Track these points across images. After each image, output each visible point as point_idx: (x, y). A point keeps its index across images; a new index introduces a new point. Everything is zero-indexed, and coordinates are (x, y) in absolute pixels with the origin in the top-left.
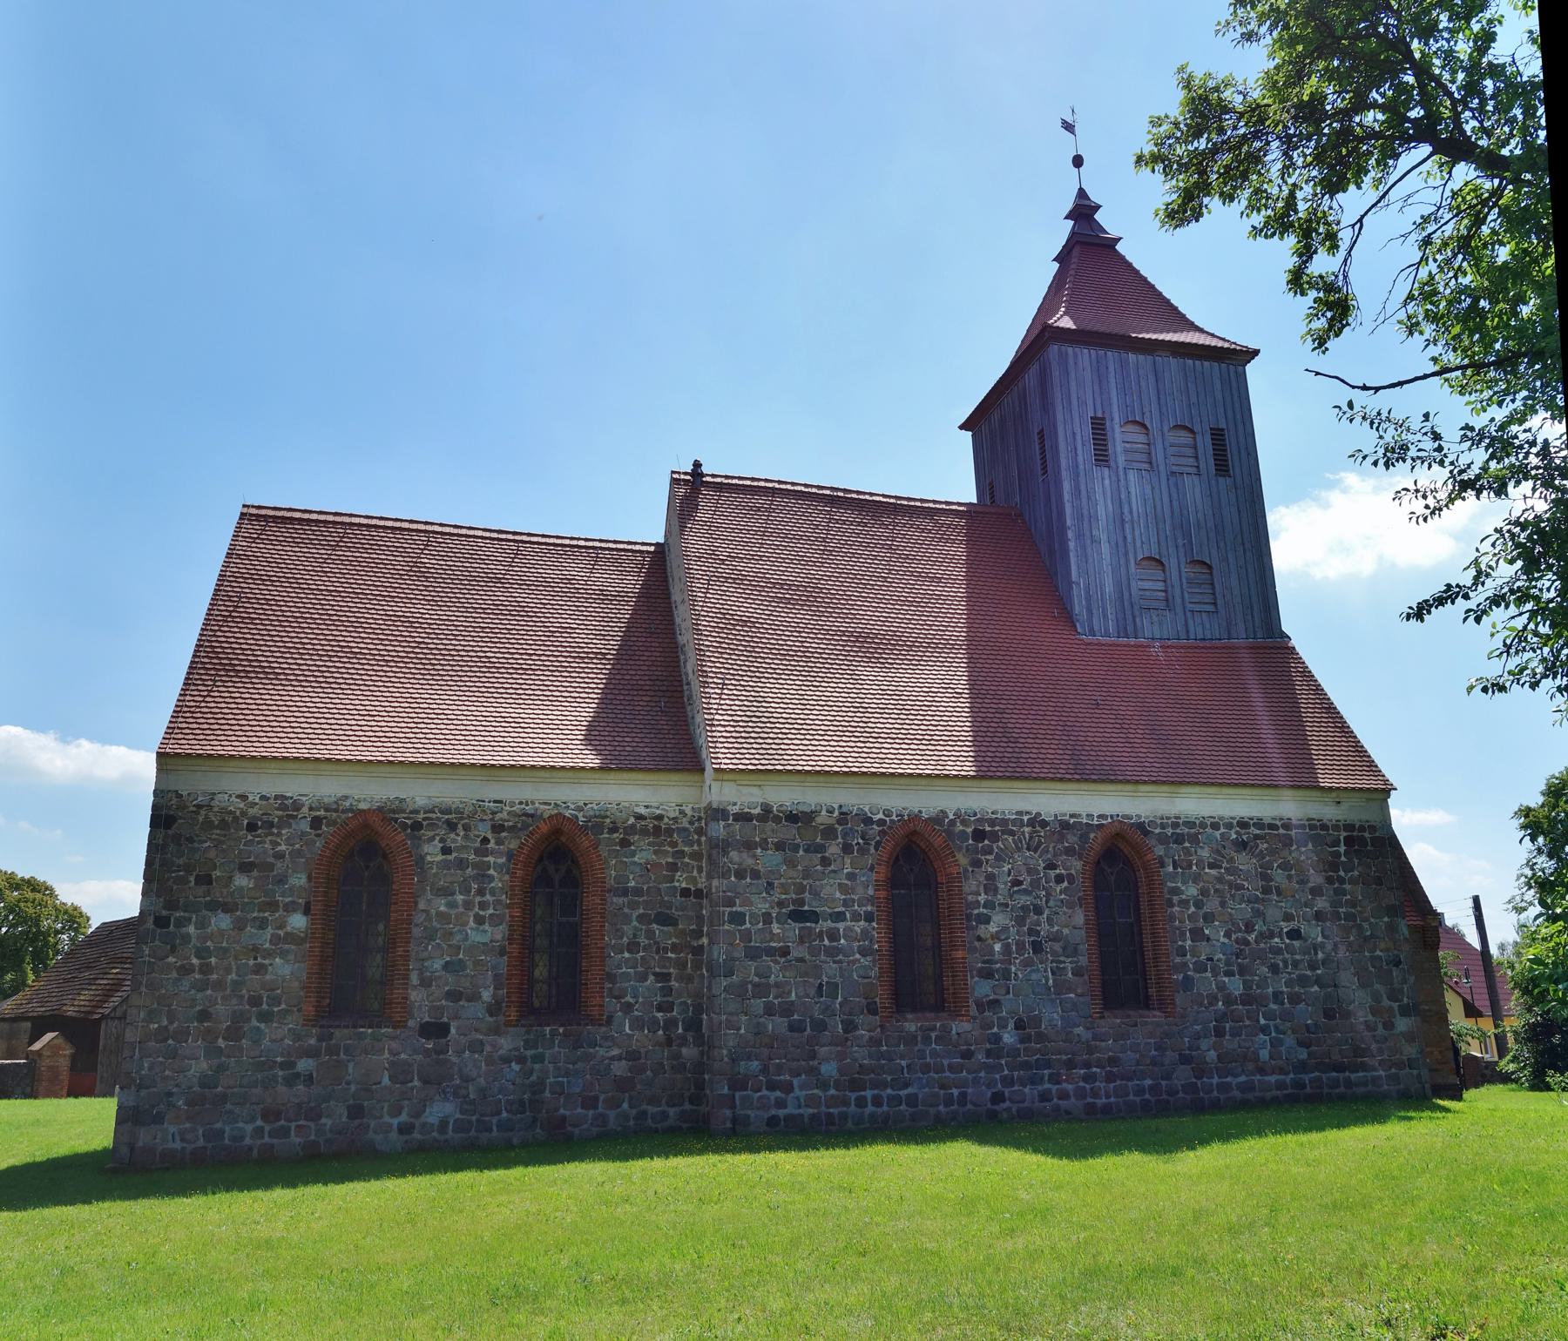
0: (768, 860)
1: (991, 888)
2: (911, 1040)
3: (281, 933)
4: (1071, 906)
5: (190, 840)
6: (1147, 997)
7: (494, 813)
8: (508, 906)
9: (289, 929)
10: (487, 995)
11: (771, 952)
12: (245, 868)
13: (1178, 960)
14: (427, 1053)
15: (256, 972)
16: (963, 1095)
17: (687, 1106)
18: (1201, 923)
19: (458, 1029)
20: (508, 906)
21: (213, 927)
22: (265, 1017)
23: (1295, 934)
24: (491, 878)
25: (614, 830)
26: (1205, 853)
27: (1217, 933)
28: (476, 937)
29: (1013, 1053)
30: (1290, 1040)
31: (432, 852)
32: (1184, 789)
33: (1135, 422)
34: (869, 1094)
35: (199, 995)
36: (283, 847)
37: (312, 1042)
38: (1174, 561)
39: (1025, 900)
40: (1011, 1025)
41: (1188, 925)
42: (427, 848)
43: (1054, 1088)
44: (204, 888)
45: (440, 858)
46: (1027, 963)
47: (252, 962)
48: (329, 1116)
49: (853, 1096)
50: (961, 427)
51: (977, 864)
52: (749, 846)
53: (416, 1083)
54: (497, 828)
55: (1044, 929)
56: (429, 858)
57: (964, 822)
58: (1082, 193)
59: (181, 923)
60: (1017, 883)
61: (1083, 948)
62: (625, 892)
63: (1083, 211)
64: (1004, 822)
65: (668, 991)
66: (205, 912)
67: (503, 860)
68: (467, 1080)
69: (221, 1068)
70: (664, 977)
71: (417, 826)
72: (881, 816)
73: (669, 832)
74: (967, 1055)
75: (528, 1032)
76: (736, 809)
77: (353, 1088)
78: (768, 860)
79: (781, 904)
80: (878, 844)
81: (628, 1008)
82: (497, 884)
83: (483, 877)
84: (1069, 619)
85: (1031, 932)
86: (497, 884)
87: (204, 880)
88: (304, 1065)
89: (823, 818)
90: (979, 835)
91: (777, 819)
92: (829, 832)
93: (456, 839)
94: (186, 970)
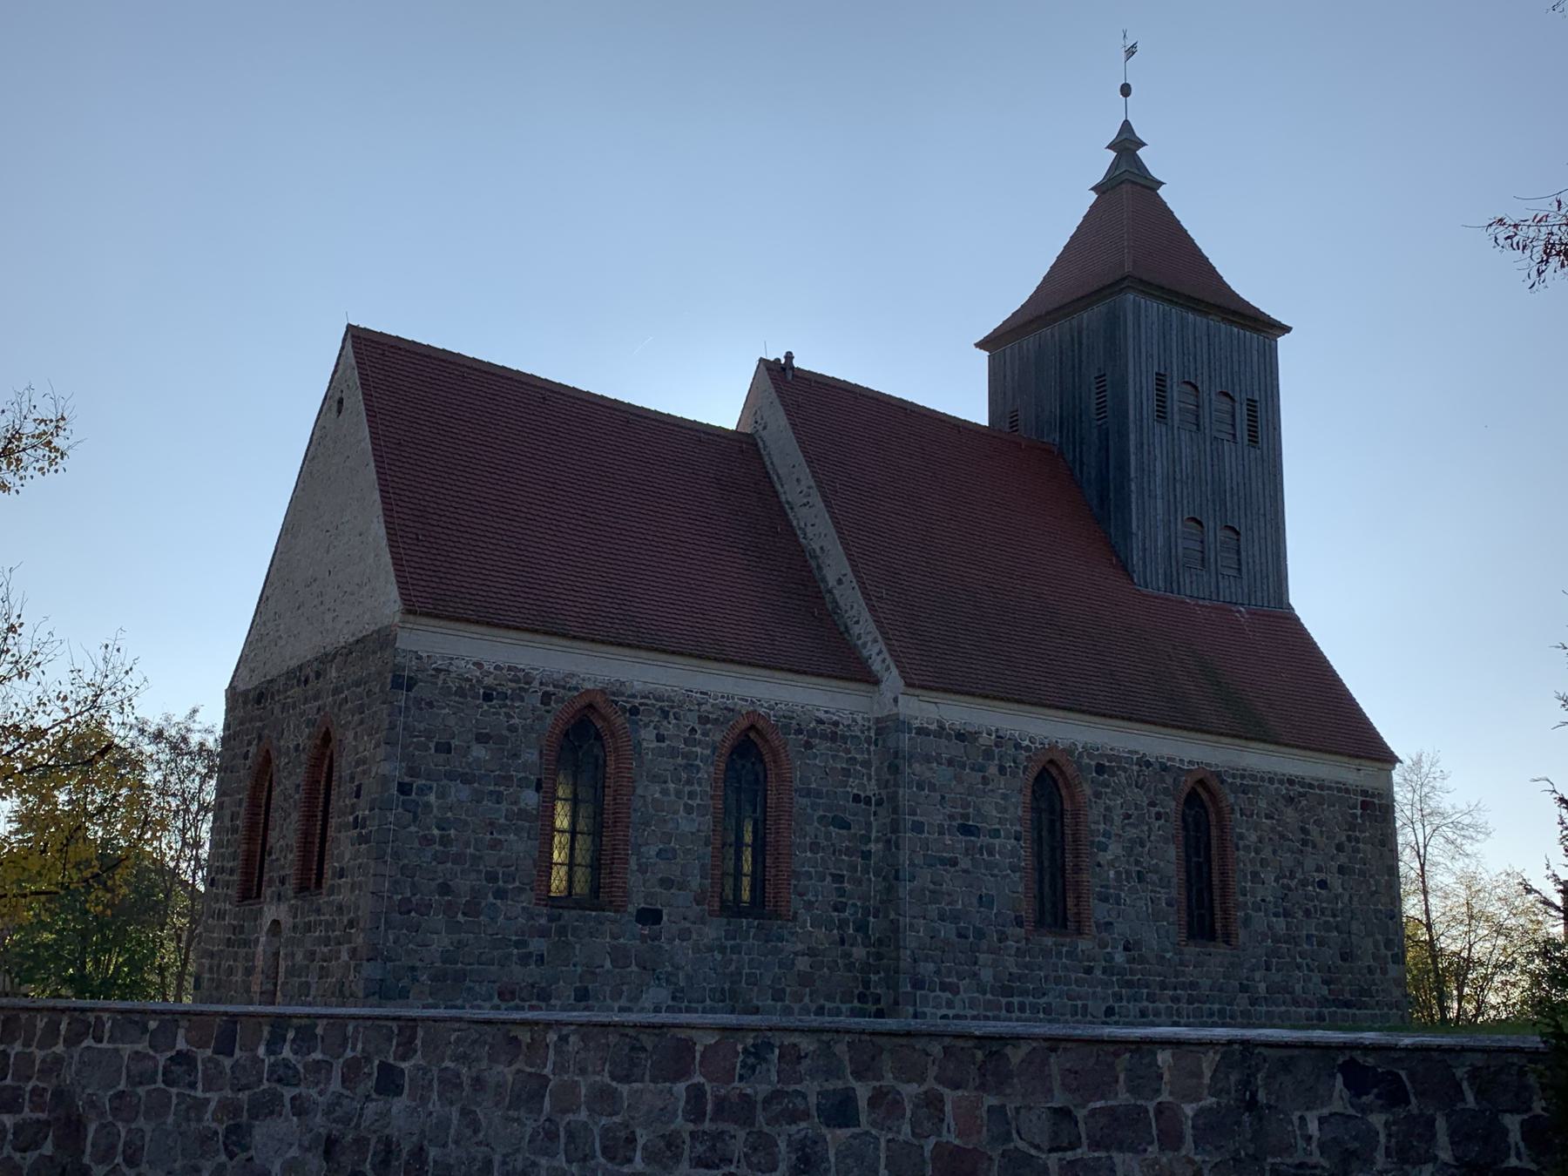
0: (941, 774)
1: (1107, 819)
2: (1046, 953)
3: (515, 809)
4: (1166, 841)
5: (430, 704)
7: (699, 704)
8: (712, 798)
9: (522, 805)
10: (695, 884)
11: (943, 862)
12: (482, 739)
13: (1241, 899)
14: (643, 938)
15: (492, 847)
16: (1085, 1007)
17: (856, 1003)
18: (1258, 868)
19: (669, 915)
20: (712, 798)
21: (452, 799)
22: (500, 894)
23: (1323, 884)
24: (698, 769)
25: (799, 731)
26: (1263, 804)
27: (1269, 876)
28: (686, 827)
29: (1122, 972)
30: (1316, 977)
31: (647, 736)
32: (1253, 744)
33: (1189, 383)
34: (1016, 1000)
35: (440, 867)
36: (517, 721)
37: (543, 921)
38: (1211, 524)
39: (1133, 833)
40: (1121, 948)
41: (1249, 868)
42: (644, 734)
43: (1151, 1006)
44: (444, 756)
45: (655, 744)
46: (1133, 890)
47: (488, 837)
48: (558, 998)
49: (1004, 1001)
50: (980, 345)
51: (1098, 795)
52: (927, 759)
53: (634, 968)
54: (703, 720)
55: (1145, 860)
56: (645, 744)
57: (1090, 756)
58: (1126, 126)
59: (422, 791)
60: (1128, 817)
61: (1175, 880)
62: (808, 793)
63: (1126, 144)
64: (1118, 758)
65: (841, 892)
66: (445, 782)
67: (708, 752)
68: (678, 968)
69: (460, 945)
70: (838, 878)
71: (634, 711)
72: (1027, 743)
73: (844, 739)
74: (1089, 970)
75: (729, 924)
76: (917, 723)
77: (579, 969)
78: (941, 774)
79: (952, 817)
80: (1026, 768)
81: (809, 905)
82: (703, 775)
84: (1124, 568)
85: (1137, 863)
86: (703, 775)
87: (444, 748)
88: (537, 945)
89: (985, 740)
90: (1100, 769)
91: (948, 737)
92: (988, 754)
93: (669, 728)
94: (427, 840)
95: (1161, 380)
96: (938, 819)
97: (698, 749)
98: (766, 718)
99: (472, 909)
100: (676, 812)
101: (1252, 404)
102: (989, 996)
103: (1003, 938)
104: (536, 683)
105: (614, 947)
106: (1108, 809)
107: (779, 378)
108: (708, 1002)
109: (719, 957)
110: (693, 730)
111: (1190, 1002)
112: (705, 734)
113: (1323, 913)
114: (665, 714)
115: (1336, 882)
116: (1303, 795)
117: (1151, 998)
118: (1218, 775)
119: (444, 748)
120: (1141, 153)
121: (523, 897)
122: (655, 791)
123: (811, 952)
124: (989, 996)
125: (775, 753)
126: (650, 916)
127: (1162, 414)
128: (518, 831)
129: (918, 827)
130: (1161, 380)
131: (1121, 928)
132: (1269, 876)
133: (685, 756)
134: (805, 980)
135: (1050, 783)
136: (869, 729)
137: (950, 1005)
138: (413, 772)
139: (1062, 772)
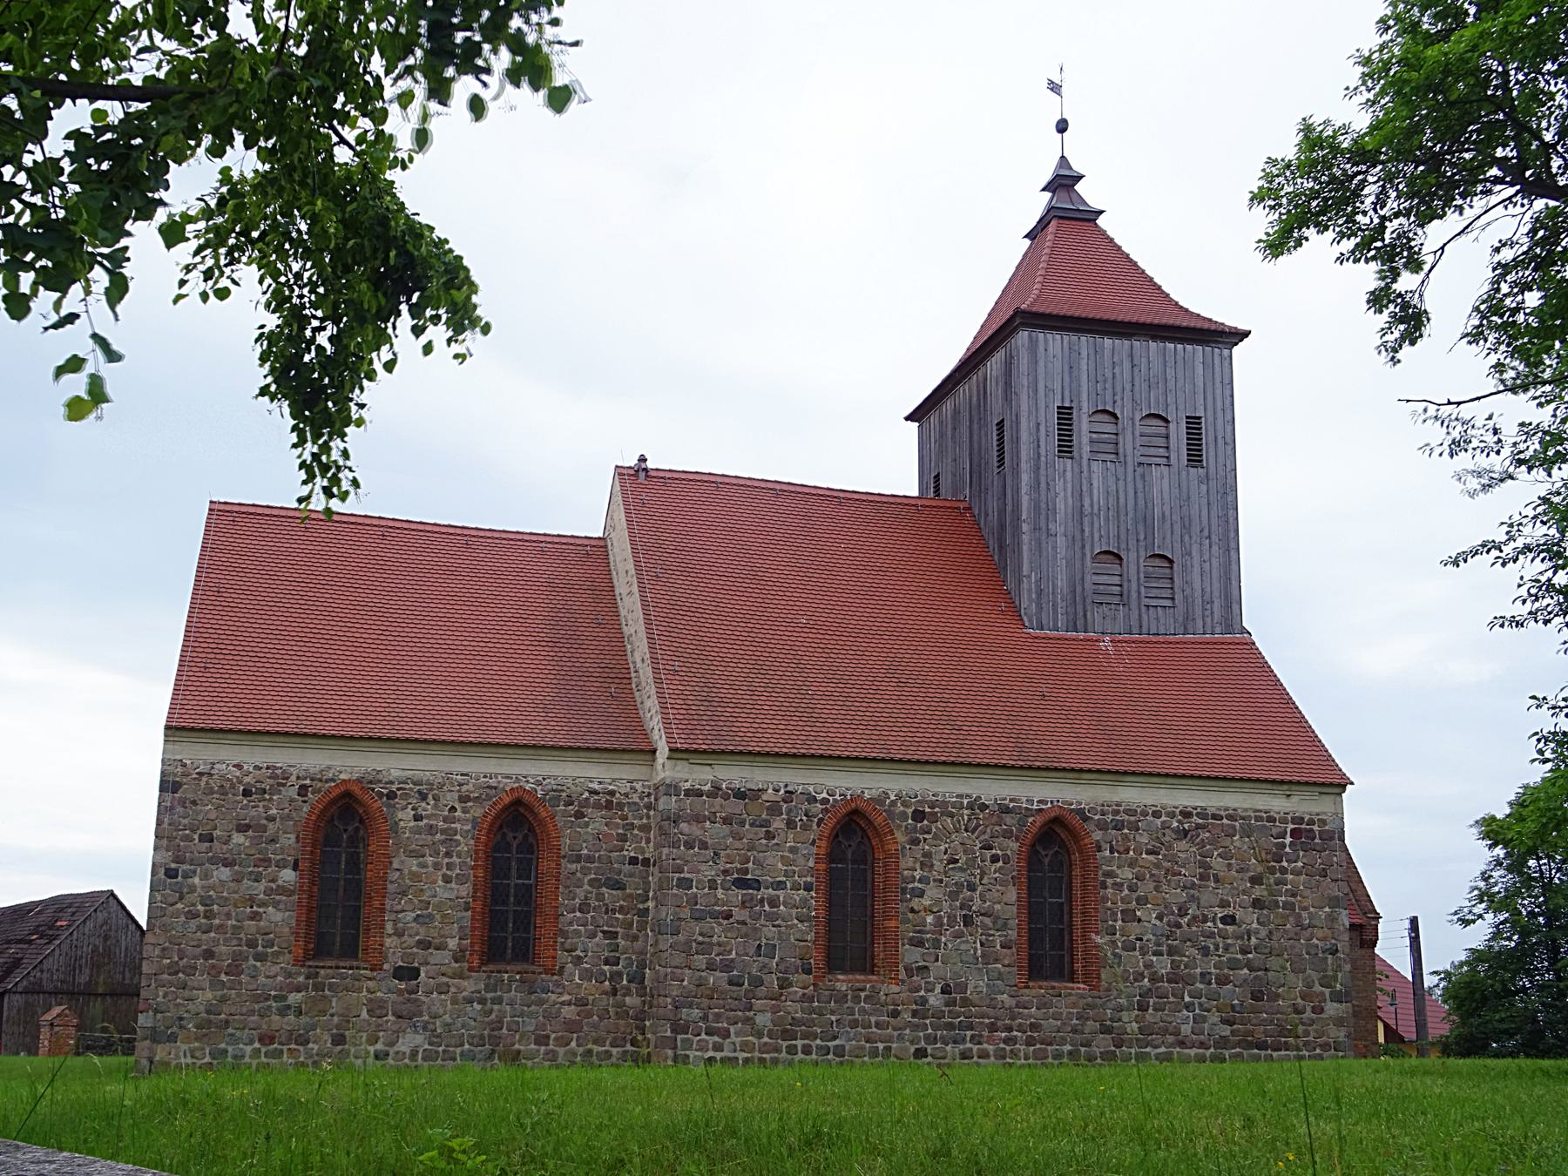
0: (715, 832)
1: (926, 864)
5: (194, 803)
6: (874, 965)
8: (473, 868)
10: (452, 944)
12: (242, 829)
14: (400, 992)
15: (252, 919)
16: (888, 1049)
20: (473, 868)
23: (1229, 920)
24: (458, 843)
26: (1144, 839)
27: (1148, 914)
29: (939, 1015)
30: (1214, 1018)
31: (405, 816)
34: (799, 1043)
35: (204, 937)
37: (301, 979)
38: (1133, 556)
39: (959, 877)
40: (938, 989)
43: (976, 1048)
45: (412, 824)
51: (915, 842)
52: (698, 819)
53: (390, 1017)
54: (464, 799)
62: (578, 859)
63: (1064, 182)
64: (945, 804)
70: (614, 935)
71: (391, 796)
72: (824, 795)
73: (620, 806)
76: (687, 785)
78: (715, 832)
79: (725, 872)
83: (450, 839)
87: (209, 838)
90: (919, 816)
92: (774, 809)
93: (427, 808)
95: (1065, 414)
96: (708, 872)
97: (457, 826)
98: (533, 792)
99: (235, 970)
100: (435, 882)
101: (1194, 424)
102: (766, 1039)
103: (784, 984)
104: (293, 778)
105: (370, 1000)
106: (927, 855)
107: (637, 482)
108: (467, 1046)
109: (477, 1006)
110: (453, 809)
111: (1028, 1044)
112: (465, 811)
113: (1226, 949)
114: (423, 797)
115: (1250, 919)
116: (1203, 827)
117: (976, 1040)
118: (1080, 812)
119: (209, 838)
120: (49, 123)
121: (281, 959)
122: (413, 864)
123: (581, 1003)
124: (766, 1039)
125: (542, 823)
126: (407, 973)
127: (1066, 446)
128: (276, 904)
129: (685, 884)
130: (1065, 414)
131: (936, 968)
132: (1148, 914)
133: (443, 832)
134: (572, 1027)
135: (854, 836)
136: (649, 795)
137: (718, 1048)
138: (178, 860)
139: (870, 822)
